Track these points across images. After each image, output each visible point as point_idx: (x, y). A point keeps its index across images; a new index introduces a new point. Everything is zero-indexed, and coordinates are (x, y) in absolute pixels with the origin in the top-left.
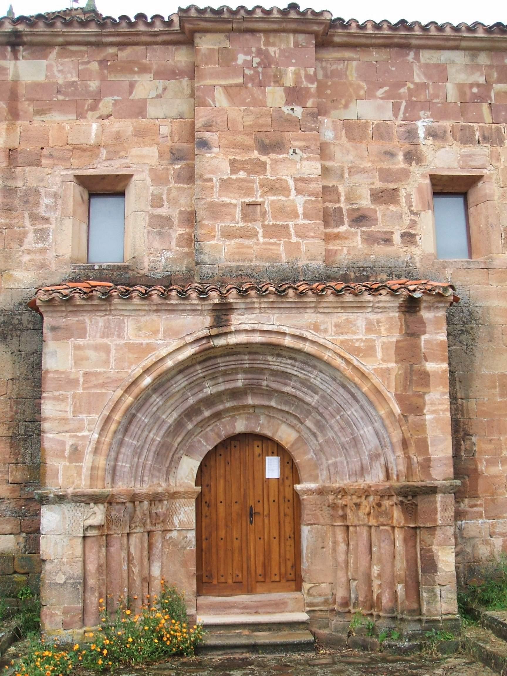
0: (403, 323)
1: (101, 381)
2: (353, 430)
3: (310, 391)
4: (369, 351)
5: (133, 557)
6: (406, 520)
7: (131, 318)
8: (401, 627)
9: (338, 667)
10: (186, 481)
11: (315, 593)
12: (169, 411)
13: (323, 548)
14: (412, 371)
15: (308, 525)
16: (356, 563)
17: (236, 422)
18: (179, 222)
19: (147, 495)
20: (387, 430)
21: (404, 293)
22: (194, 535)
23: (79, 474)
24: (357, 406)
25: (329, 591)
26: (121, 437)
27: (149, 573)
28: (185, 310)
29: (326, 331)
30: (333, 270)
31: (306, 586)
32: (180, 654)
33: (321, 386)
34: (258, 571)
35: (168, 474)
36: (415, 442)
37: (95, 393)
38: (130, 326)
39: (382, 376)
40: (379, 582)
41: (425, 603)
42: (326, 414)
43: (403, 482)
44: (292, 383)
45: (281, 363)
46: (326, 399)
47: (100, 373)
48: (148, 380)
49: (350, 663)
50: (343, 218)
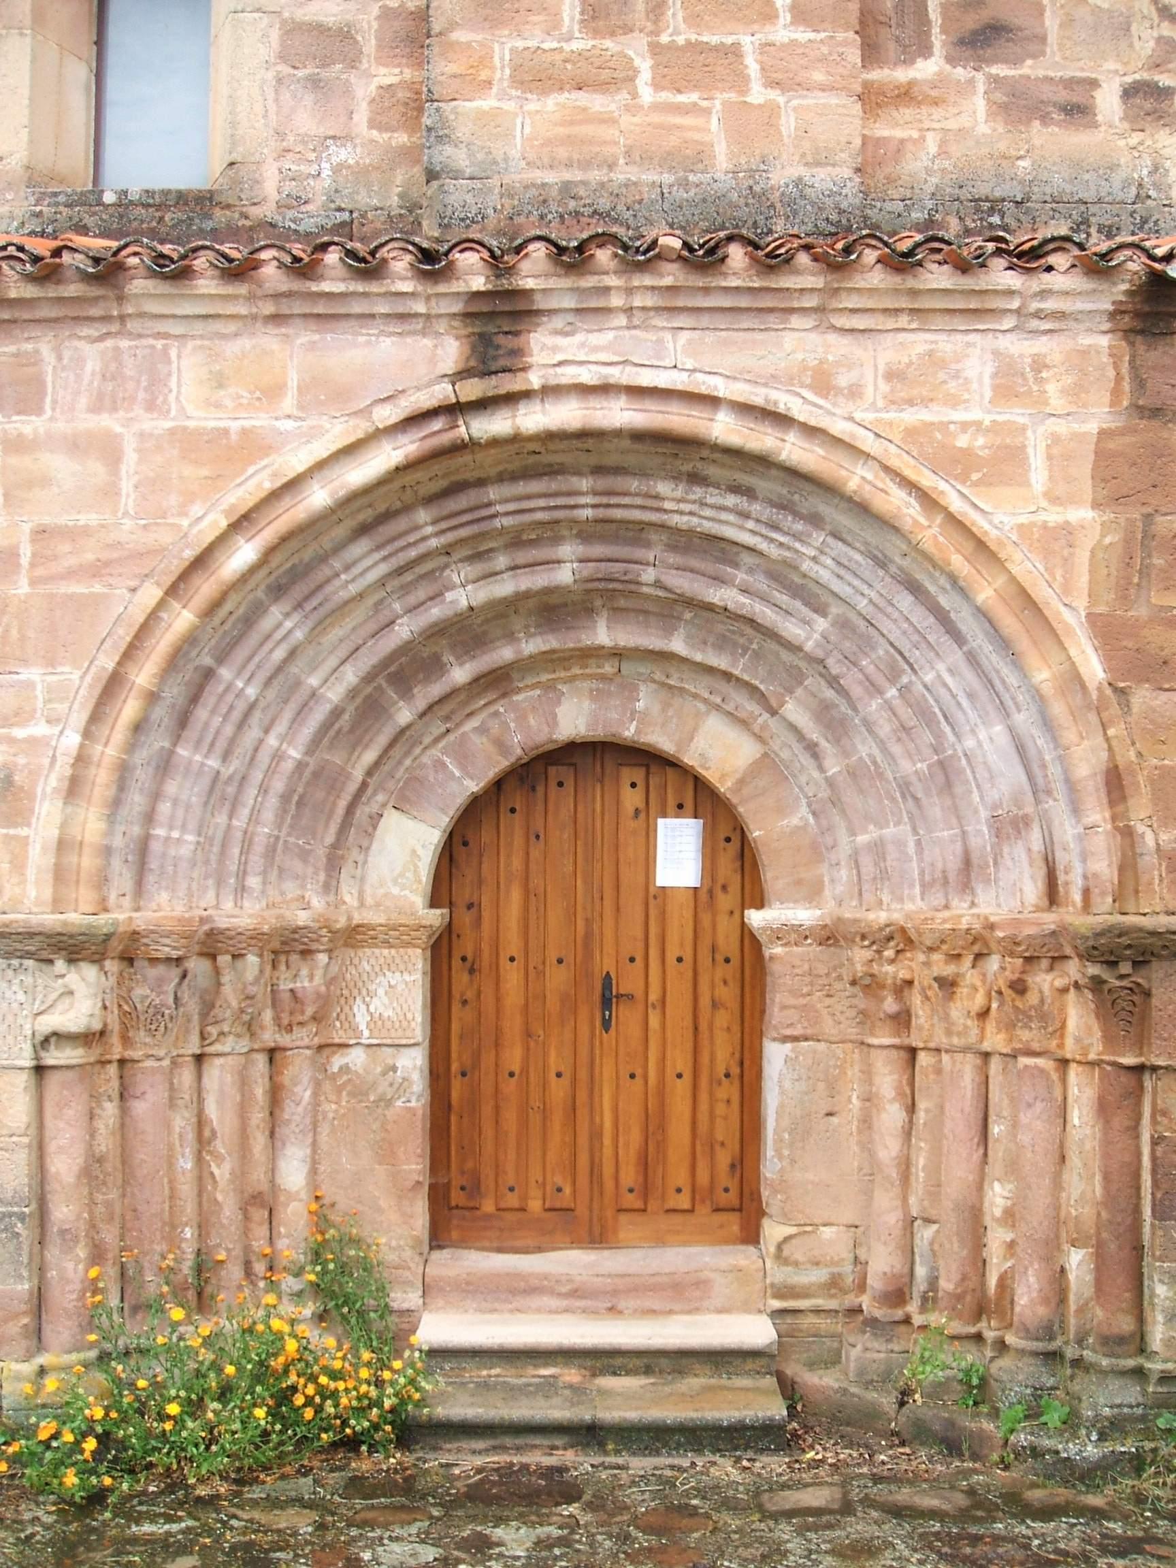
0: (1125, 369)
1: (90, 557)
2: (939, 736)
3: (798, 604)
4: (1005, 463)
5: (214, 1133)
6: (1109, 1039)
7: (190, 345)
8: (1075, 1387)
9: (858, 1528)
10: (395, 891)
11: (798, 1256)
12: (333, 662)
13: (830, 1114)
14: (1148, 535)
15: (785, 1039)
16: (935, 1168)
17: (559, 703)
18: (379, 47)
19: (257, 938)
20: (1055, 740)
21: (1132, 266)
22: (419, 1062)
23: (18, 865)
24: (956, 656)
25: (843, 1251)
26: (167, 744)
27: (272, 1181)
28: (373, 316)
29: (854, 392)
30: (888, 206)
31: (773, 1231)
32: (351, 1444)
33: (836, 586)
34: (622, 1174)
35: (334, 864)
36: (1151, 781)
37: (71, 597)
38: (187, 368)
39: (1047, 554)
40: (1009, 1237)
41: (1160, 1318)
42: (852, 680)
43: (1104, 915)
44: (741, 576)
45: (703, 504)
46: (855, 631)
47: (86, 531)
48: (243, 555)
49: (898, 1512)
50: (928, 34)
